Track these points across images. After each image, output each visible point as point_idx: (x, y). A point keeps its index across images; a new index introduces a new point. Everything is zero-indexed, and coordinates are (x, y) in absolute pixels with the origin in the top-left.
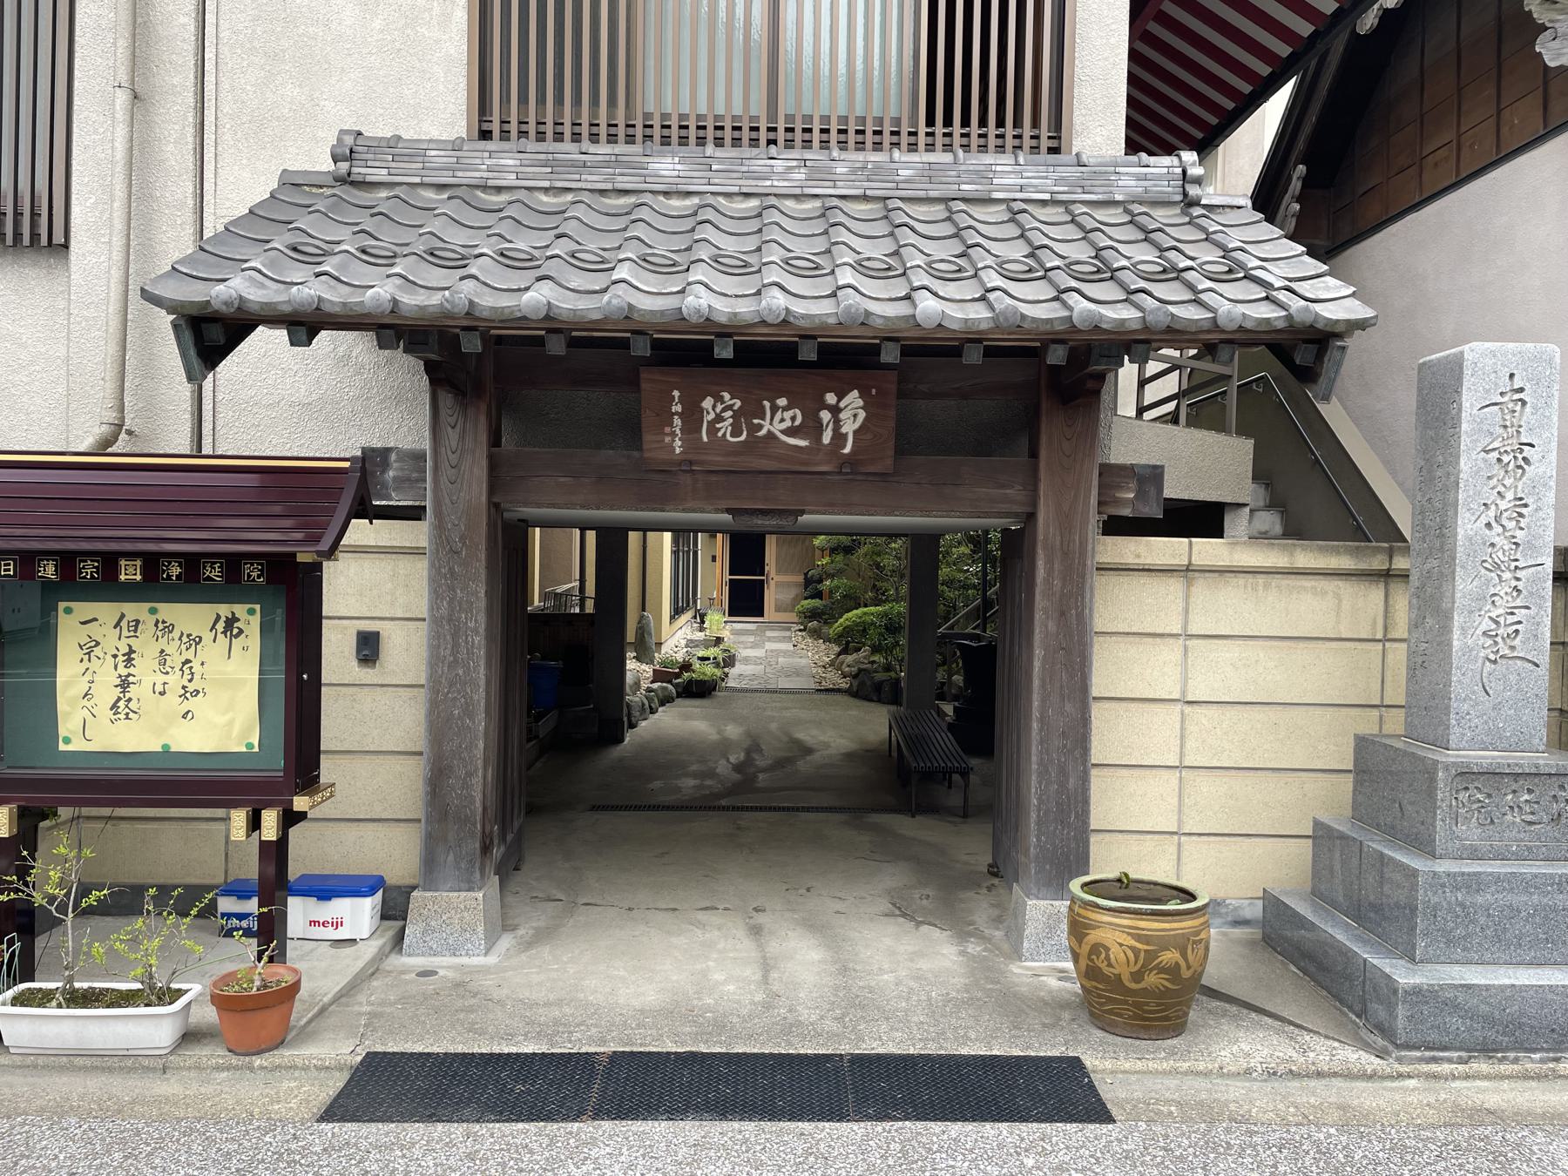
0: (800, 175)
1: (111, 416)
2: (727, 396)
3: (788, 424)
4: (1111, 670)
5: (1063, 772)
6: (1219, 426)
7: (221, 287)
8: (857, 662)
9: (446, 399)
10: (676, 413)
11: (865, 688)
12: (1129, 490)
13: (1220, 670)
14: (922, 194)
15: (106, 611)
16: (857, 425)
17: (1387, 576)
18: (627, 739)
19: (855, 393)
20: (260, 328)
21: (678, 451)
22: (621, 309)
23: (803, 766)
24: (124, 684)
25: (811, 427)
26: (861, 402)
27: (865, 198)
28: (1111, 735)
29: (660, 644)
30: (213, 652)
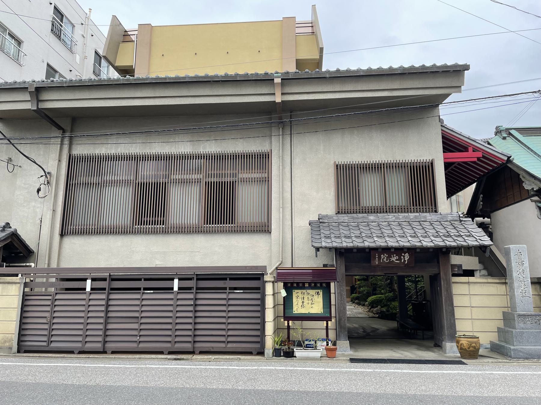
0: (394, 218)
4: (457, 301)
5: (450, 320)
8: (378, 310)
11: (383, 316)
13: (476, 301)
15: (300, 291)
17: (506, 283)
24: (303, 302)
25: (400, 259)
28: (458, 313)
30: (316, 297)
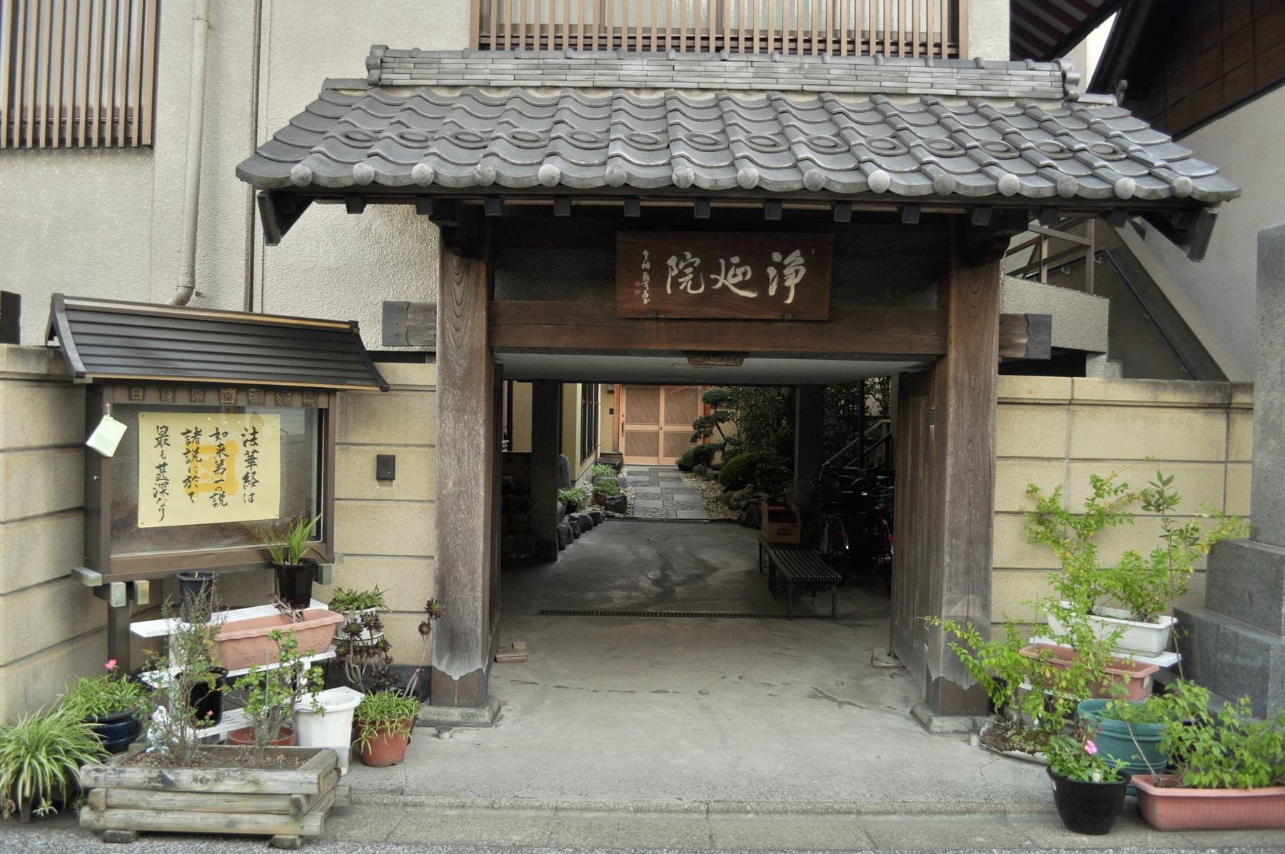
1: (183, 280)
2: (688, 255)
3: (740, 278)
6: (1080, 286)
7: (298, 166)
9: (454, 261)
10: (646, 270)
12: (1022, 336)
14: (850, 89)
16: (798, 280)
18: (560, 557)
19: (798, 252)
20: (314, 204)
21: (646, 301)
22: (621, 177)
23: (712, 581)
25: (759, 282)
26: (801, 260)
27: (802, 92)
29: (574, 482)
